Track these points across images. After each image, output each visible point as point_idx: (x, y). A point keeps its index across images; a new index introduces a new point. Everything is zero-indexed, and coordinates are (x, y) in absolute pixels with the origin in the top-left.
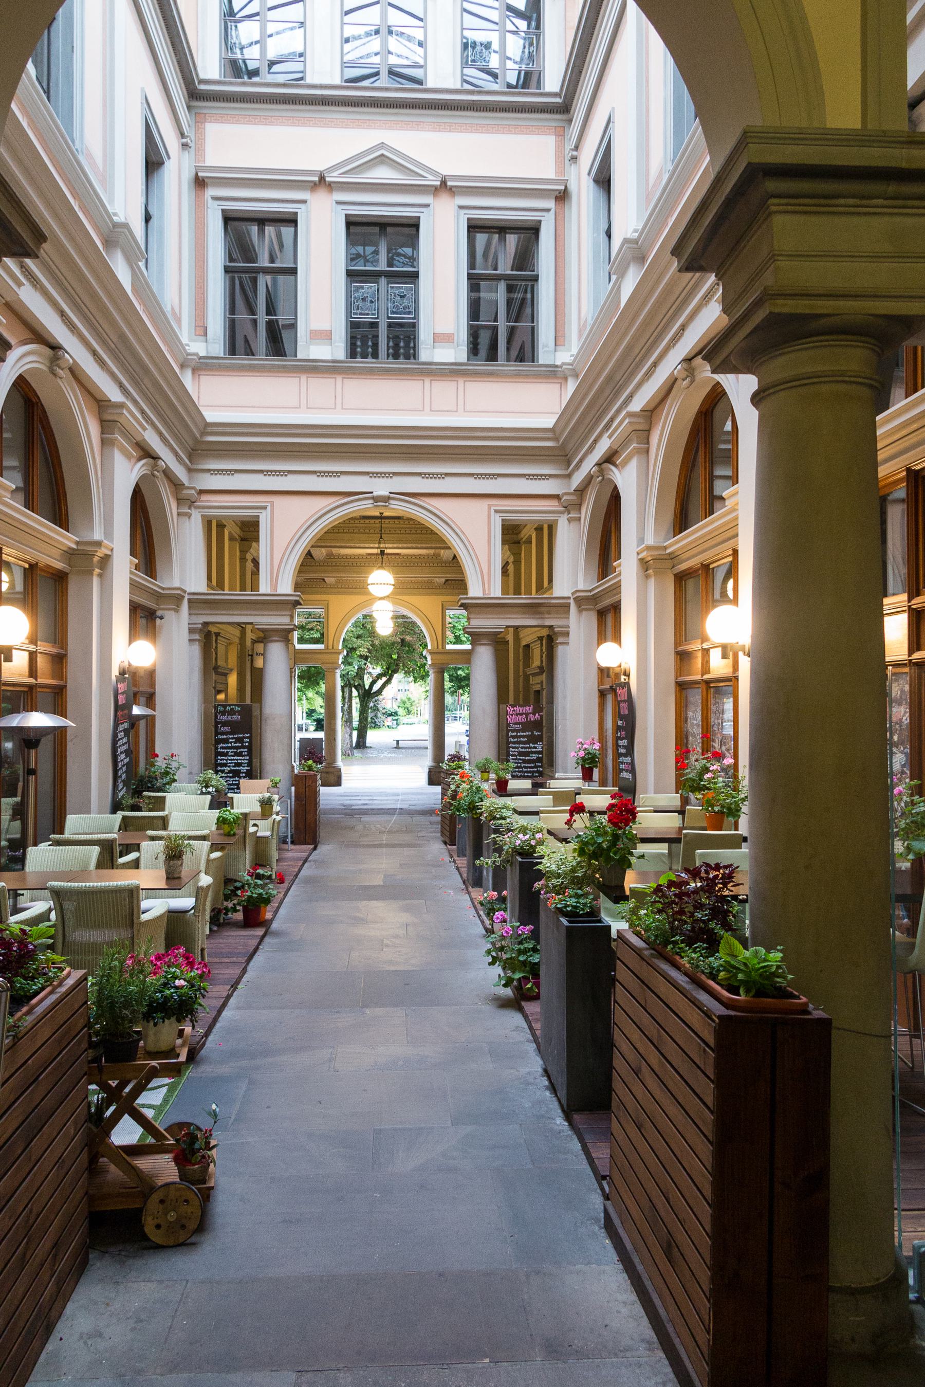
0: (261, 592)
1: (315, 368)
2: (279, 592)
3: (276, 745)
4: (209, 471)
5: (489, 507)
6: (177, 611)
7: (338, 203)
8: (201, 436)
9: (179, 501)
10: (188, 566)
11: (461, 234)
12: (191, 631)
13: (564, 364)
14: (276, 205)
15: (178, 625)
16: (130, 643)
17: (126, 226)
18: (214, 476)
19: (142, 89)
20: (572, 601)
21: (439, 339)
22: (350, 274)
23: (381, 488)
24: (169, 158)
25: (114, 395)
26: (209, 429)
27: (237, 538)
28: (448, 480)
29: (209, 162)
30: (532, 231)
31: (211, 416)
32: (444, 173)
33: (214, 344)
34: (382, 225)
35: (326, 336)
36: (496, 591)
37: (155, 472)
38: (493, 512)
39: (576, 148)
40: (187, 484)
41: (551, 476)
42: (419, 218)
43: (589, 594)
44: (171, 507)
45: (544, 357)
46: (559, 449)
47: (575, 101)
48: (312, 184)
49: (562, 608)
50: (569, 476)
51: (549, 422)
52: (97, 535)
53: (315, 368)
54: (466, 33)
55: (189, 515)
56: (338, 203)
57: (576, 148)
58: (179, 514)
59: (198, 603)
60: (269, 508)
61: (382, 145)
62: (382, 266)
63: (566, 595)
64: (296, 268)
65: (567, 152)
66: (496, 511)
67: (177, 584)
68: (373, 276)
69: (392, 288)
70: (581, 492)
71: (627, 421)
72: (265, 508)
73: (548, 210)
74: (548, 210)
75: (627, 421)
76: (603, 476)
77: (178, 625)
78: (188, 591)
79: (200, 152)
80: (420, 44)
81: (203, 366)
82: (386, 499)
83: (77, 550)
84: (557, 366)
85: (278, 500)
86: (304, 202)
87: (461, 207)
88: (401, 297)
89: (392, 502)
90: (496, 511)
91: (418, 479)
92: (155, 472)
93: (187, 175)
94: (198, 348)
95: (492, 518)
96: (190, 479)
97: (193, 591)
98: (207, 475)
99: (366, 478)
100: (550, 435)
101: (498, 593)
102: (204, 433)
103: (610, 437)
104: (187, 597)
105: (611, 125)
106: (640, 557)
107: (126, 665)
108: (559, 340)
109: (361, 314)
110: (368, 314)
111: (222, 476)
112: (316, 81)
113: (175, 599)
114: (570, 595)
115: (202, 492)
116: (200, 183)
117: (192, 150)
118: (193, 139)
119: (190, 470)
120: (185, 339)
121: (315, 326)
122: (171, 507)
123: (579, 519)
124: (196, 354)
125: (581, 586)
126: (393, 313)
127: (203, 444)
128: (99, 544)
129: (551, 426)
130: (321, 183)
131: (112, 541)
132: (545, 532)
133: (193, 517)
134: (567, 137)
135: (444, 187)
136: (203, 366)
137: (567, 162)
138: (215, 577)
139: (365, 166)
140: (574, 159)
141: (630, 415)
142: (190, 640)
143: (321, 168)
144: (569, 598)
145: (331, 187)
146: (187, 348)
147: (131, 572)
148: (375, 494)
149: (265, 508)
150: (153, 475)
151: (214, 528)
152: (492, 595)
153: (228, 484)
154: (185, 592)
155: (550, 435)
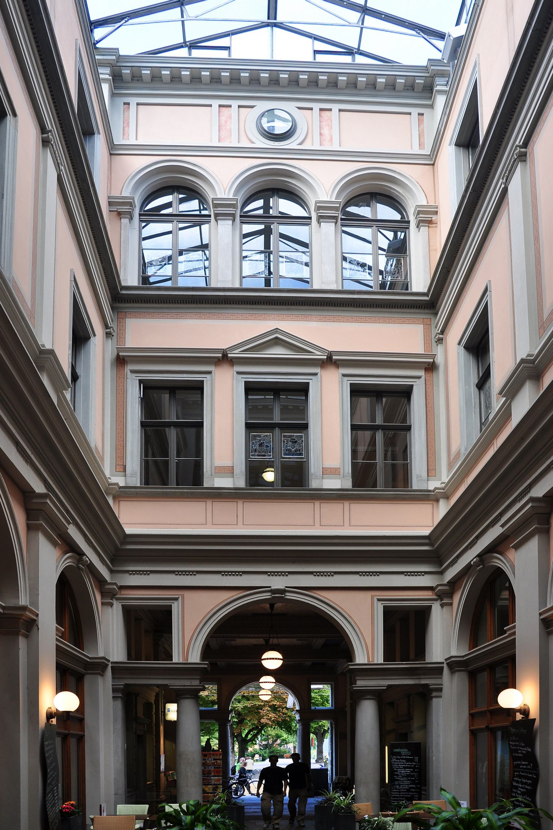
0: (174, 661)
1: (220, 495)
2: (189, 661)
3: (189, 774)
4: (128, 572)
5: (372, 597)
6: (102, 675)
7: (238, 373)
8: (121, 545)
9: (103, 594)
10: (111, 639)
11: (345, 394)
12: (114, 690)
13: (436, 488)
14: (185, 375)
15: (104, 687)
16: (57, 693)
17: (51, 352)
18: (132, 576)
19: (72, 270)
20: (445, 666)
21: (327, 472)
22: (249, 427)
23: (278, 583)
24: (95, 335)
25: (38, 487)
26: (129, 540)
27: (150, 627)
28: (336, 577)
29: (128, 345)
30: (406, 393)
31: (129, 530)
32: (330, 350)
33: (133, 476)
34: (277, 390)
35: (230, 471)
36: (379, 658)
37: (81, 566)
38: (376, 600)
39: (442, 332)
40: (109, 580)
41: (426, 573)
42: (309, 383)
43: (462, 659)
44: (97, 598)
45: (416, 485)
46: (434, 551)
47: (440, 301)
48: (216, 360)
49: (437, 671)
50: (442, 573)
51: (426, 532)
52: (23, 600)
53: (220, 495)
54: (344, 255)
55: (111, 605)
56: (238, 373)
57: (442, 332)
58: (103, 604)
59: (118, 670)
60: (180, 599)
61: (276, 330)
62: (277, 419)
63: (439, 660)
64: (203, 423)
65: (433, 336)
66: (379, 600)
67: (101, 654)
68: (270, 427)
69: (285, 436)
70: (454, 584)
71: (530, 505)
72: (176, 599)
73: (419, 377)
74: (419, 377)
75: (530, 505)
76: (484, 565)
77: (104, 687)
78: (111, 660)
79: (121, 337)
80: (307, 264)
81: (125, 494)
82: (283, 591)
83: (4, 614)
84: (430, 491)
85: (188, 595)
86: (210, 373)
87: (344, 375)
88: (293, 442)
89: (287, 594)
90: (379, 600)
91: (311, 577)
92: (81, 566)
93: (110, 355)
94: (121, 481)
95: (375, 604)
96: (112, 578)
97: (115, 660)
98: (127, 575)
99: (265, 577)
100: (426, 541)
101: (381, 661)
102: (122, 543)
103: (503, 526)
104: (110, 665)
105: (488, 293)
106: (542, 617)
107: (53, 710)
108: (431, 471)
109: (258, 455)
110: (265, 456)
111: (139, 576)
112: (220, 285)
113: (99, 666)
114: (444, 661)
115: (122, 588)
116: (120, 361)
117: (115, 338)
118: (115, 330)
119: (112, 571)
120: (107, 473)
121: (218, 463)
122: (97, 598)
123: (451, 604)
124: (117, 484)
125: (454, 653)
126: (285, 454)
127: (125, 551)
128: (24, 608)
129: (427, 534)
130: (224, 359)
131: (38, 610)
132: (422, 616)
133: (115, 606)
134: (433, 326)
135: (330, 361)
136: (125, 494)
137: (434, 344)
138: (133, 650)
139: (262, 346)
140: (440, 341)
141: (532, 500)
142: (113, 697)
143: (224, 346)
144: (443, 663)
145: (232, 362)
146: (109, 480)
147: (57, 640)
148: (273, 588)
149: (176, 599)
150: (79, 568)
151: (131, 616)
152: (376, 662)
153: (143, 582)
154: (109, 661)
155: (426, 541)
